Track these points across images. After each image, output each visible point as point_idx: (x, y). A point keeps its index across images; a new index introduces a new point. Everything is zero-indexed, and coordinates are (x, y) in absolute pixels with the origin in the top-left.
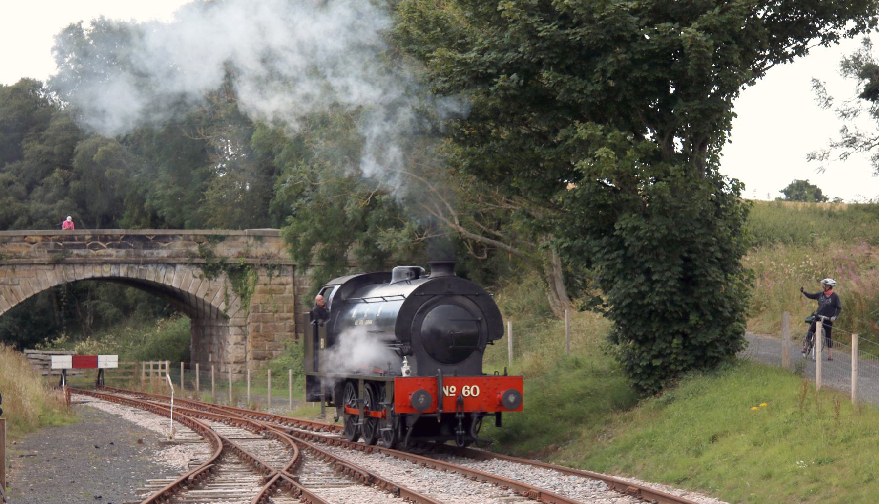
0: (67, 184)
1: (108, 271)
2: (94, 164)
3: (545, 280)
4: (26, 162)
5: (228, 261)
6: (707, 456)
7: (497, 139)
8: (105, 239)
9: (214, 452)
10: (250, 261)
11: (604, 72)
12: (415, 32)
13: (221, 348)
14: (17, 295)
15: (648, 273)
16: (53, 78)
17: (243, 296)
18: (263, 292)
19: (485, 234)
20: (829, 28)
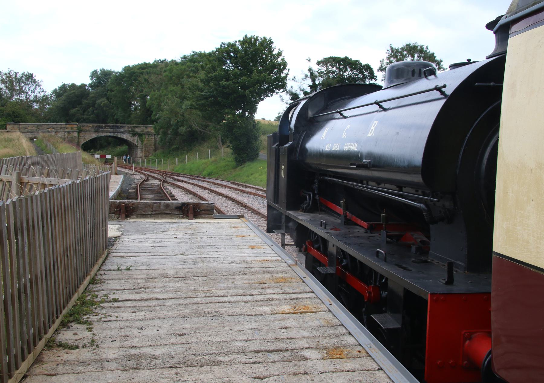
0: (94, 111)
1: (109, 134)
2: (101, 106)
3: (217, 140)
4: (83, 105)
5: (139, 133)
6: (250, 177)
7: (209, 110)
8: (108, 126)
9: (146, 177)
10: (144, 133)
11: (231, 99)
12: (191, 87)
13: (136, 154)
14: (86, 139)
15: (240, 140)
16: (90, 84)
17: (142, 141)
18: (147, 140)
19: (203, 129)
20: (277, 91)
